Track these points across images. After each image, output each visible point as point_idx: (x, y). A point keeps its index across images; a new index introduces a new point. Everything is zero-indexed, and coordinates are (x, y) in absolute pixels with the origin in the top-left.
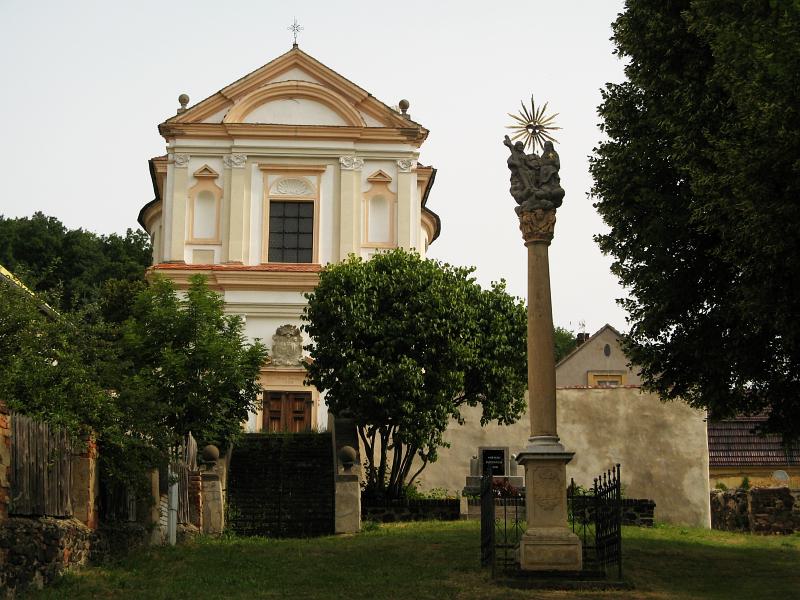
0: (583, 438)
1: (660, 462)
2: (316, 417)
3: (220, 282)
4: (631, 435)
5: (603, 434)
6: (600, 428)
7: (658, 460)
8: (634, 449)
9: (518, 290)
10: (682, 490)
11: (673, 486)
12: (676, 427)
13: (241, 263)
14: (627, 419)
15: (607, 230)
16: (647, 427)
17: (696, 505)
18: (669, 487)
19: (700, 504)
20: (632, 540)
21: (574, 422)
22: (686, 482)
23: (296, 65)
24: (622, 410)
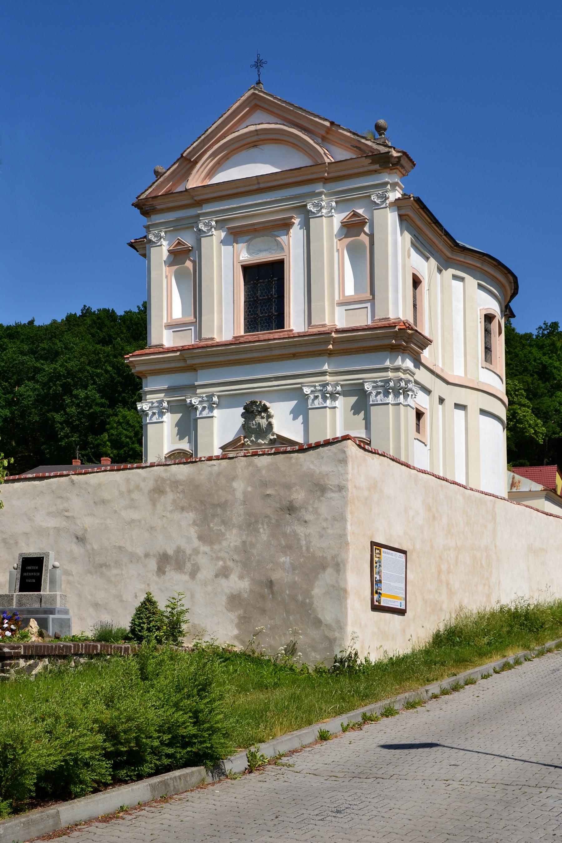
0: (193, 532)
1: (284, 563)
2: (388, 553)
3: (189, 362)
4: (249, 525)
5: (215, 525)
6: (213, 516)
7: (282, 559)
8: (253, 545)
9: (411, 321)
10: (311, 604)
11: (300, 598)
12: (306, 509)
13: (212, 339)
14: (244, 502)
15: (36, 323)
16: (269, 511)
17: (328, 626)
18: (293, 598)
19: (334, 625)
20: (16, 606)
21: (183, 509)
22: (317, 591)
23: (255, 98)
24: (239, 486)
